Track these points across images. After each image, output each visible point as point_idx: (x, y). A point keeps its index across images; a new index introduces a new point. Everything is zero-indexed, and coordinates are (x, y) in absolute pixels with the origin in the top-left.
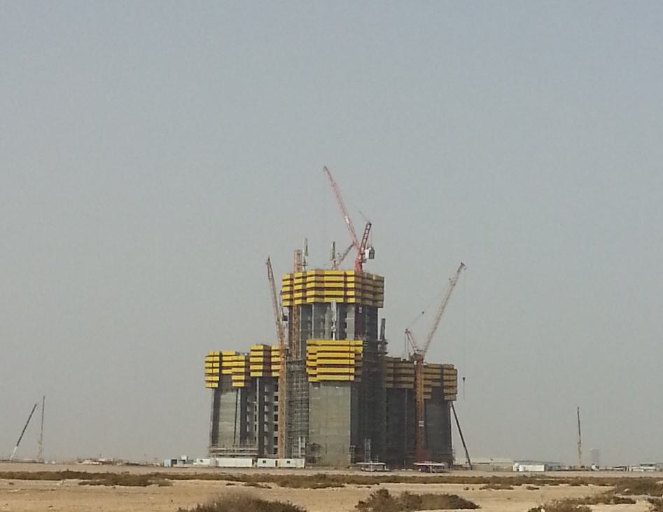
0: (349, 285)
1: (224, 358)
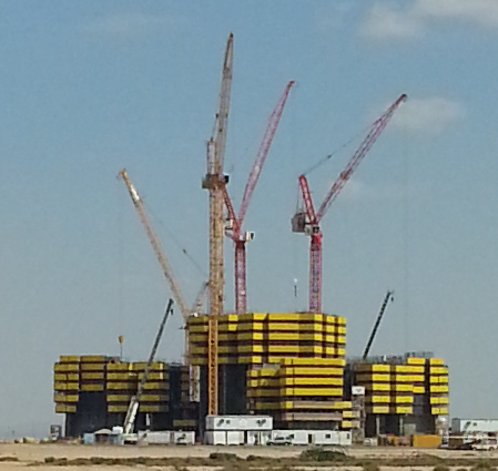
0: (258, 348)
1: (272, 326)
